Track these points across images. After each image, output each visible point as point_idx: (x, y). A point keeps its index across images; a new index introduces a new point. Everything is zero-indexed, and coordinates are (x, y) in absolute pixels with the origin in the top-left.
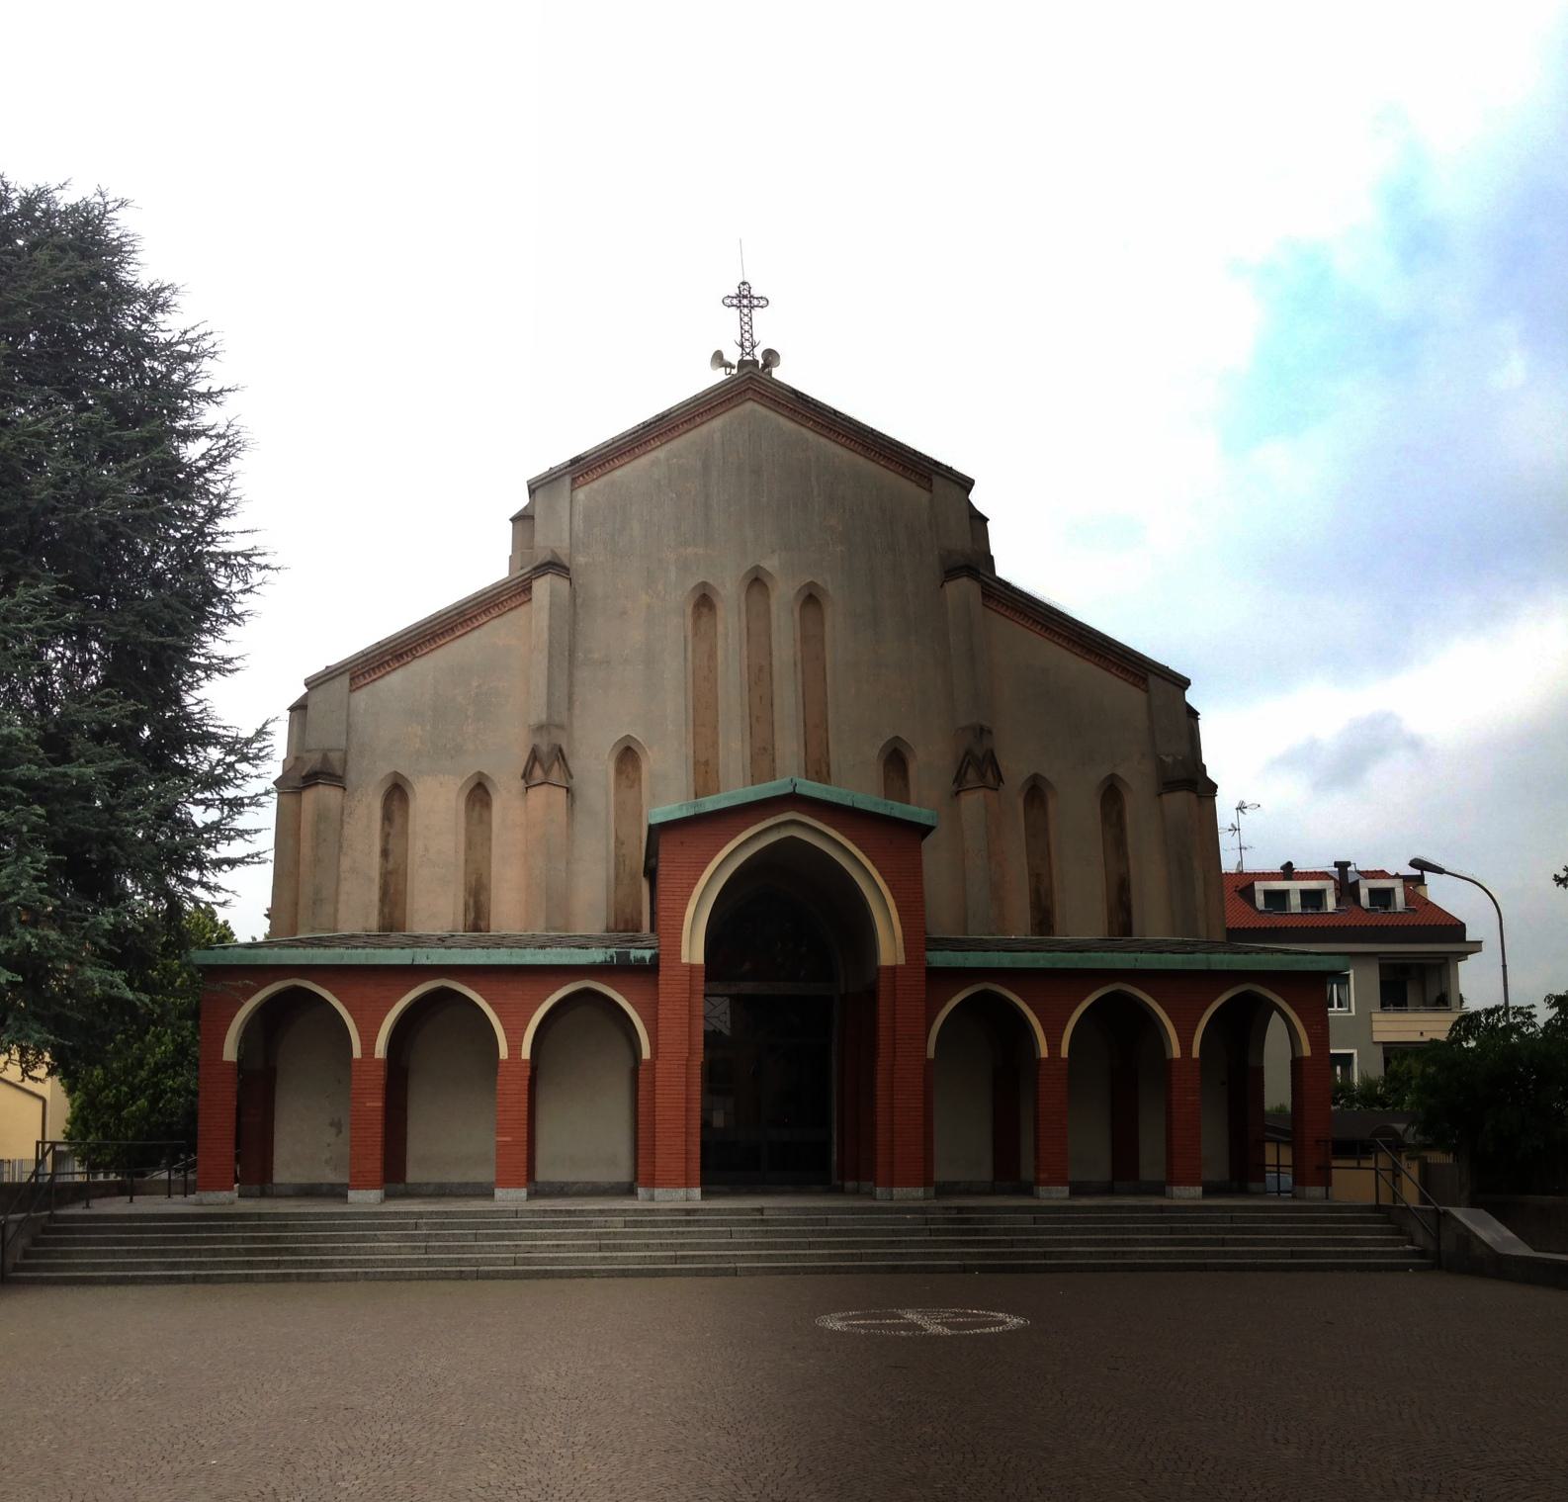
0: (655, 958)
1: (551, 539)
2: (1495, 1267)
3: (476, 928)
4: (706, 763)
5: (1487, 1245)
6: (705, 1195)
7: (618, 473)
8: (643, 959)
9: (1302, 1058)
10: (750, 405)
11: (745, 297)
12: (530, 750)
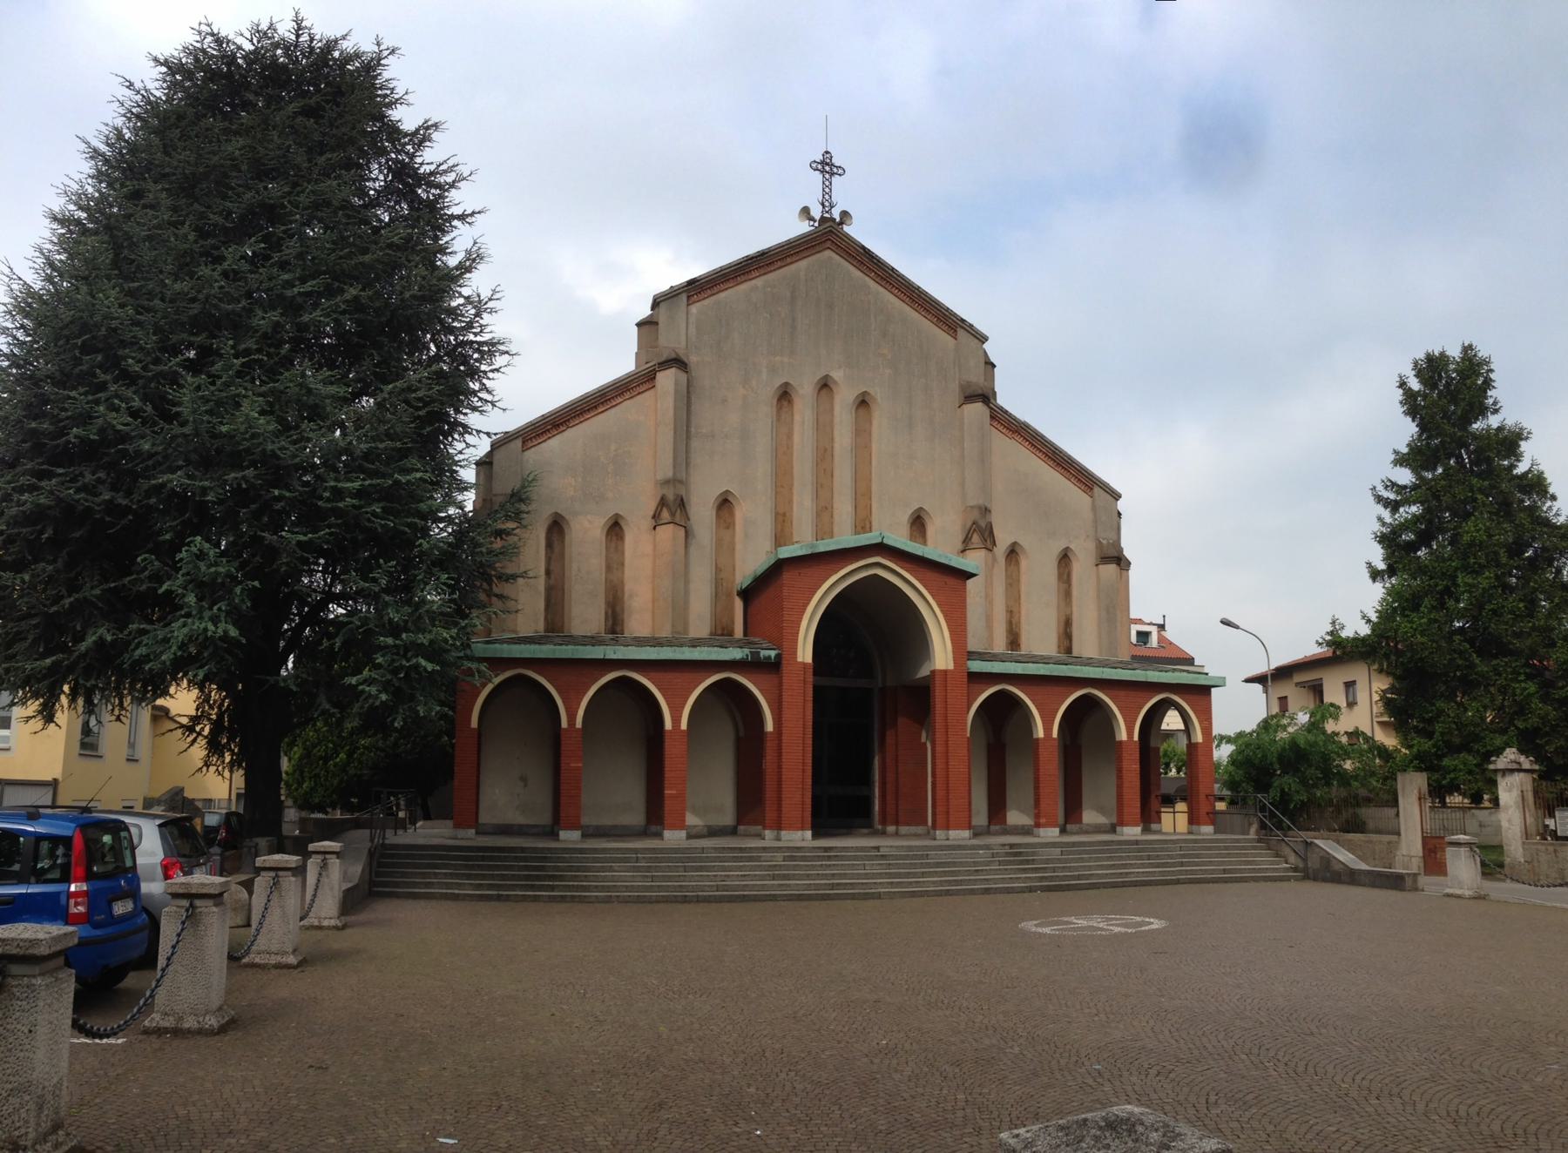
0: (779, 656)
1: (671, 340)
2: (1350, 877)
3: (613, 632)
4: (784, 515)
5: (1343, 863)
6: (815, 836)
7: (722, 295)
8: (770, 657)
9: (1197, 744)
10: (828, 253)
11: (827, 164)
12: (659, 498)
